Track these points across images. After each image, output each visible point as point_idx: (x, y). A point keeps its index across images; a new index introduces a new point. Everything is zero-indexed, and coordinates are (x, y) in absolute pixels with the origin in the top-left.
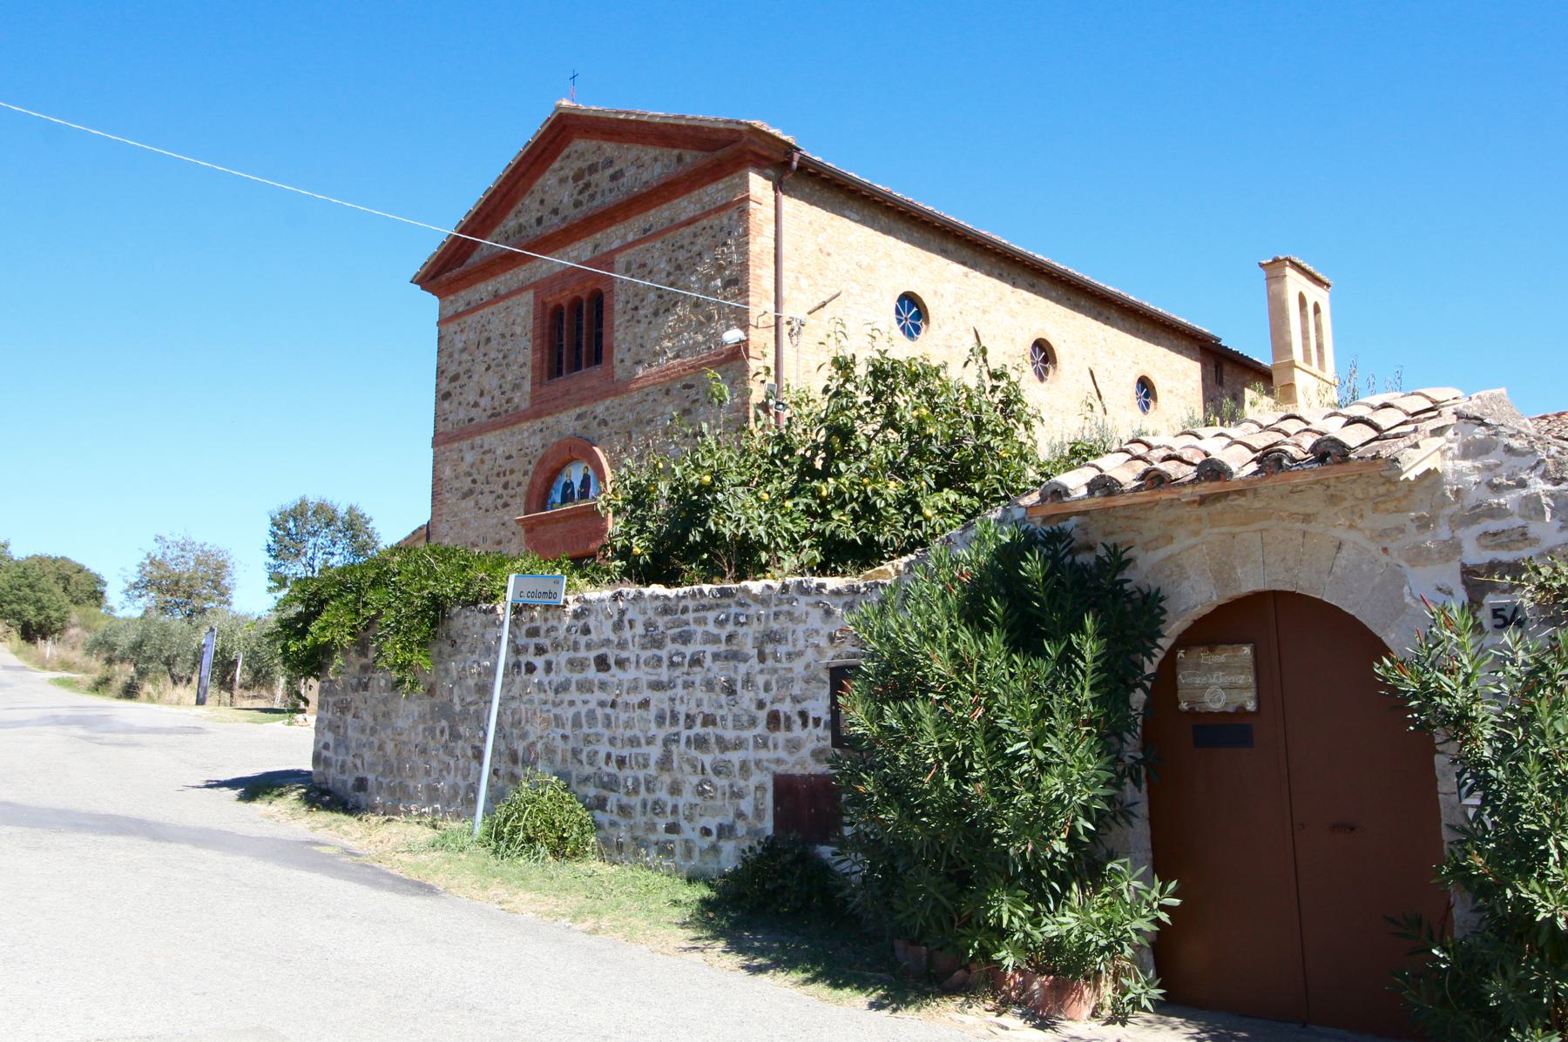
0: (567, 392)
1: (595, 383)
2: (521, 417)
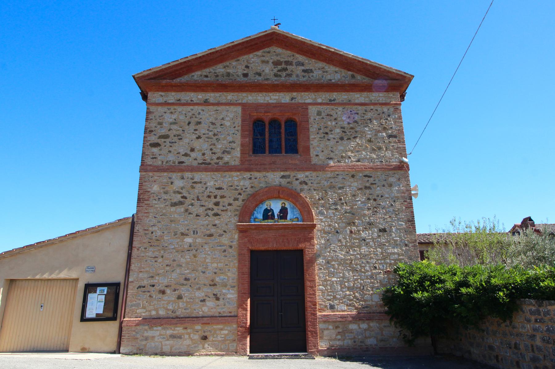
0: (274, 163)
1: (297, 162)
2: (228, 168)
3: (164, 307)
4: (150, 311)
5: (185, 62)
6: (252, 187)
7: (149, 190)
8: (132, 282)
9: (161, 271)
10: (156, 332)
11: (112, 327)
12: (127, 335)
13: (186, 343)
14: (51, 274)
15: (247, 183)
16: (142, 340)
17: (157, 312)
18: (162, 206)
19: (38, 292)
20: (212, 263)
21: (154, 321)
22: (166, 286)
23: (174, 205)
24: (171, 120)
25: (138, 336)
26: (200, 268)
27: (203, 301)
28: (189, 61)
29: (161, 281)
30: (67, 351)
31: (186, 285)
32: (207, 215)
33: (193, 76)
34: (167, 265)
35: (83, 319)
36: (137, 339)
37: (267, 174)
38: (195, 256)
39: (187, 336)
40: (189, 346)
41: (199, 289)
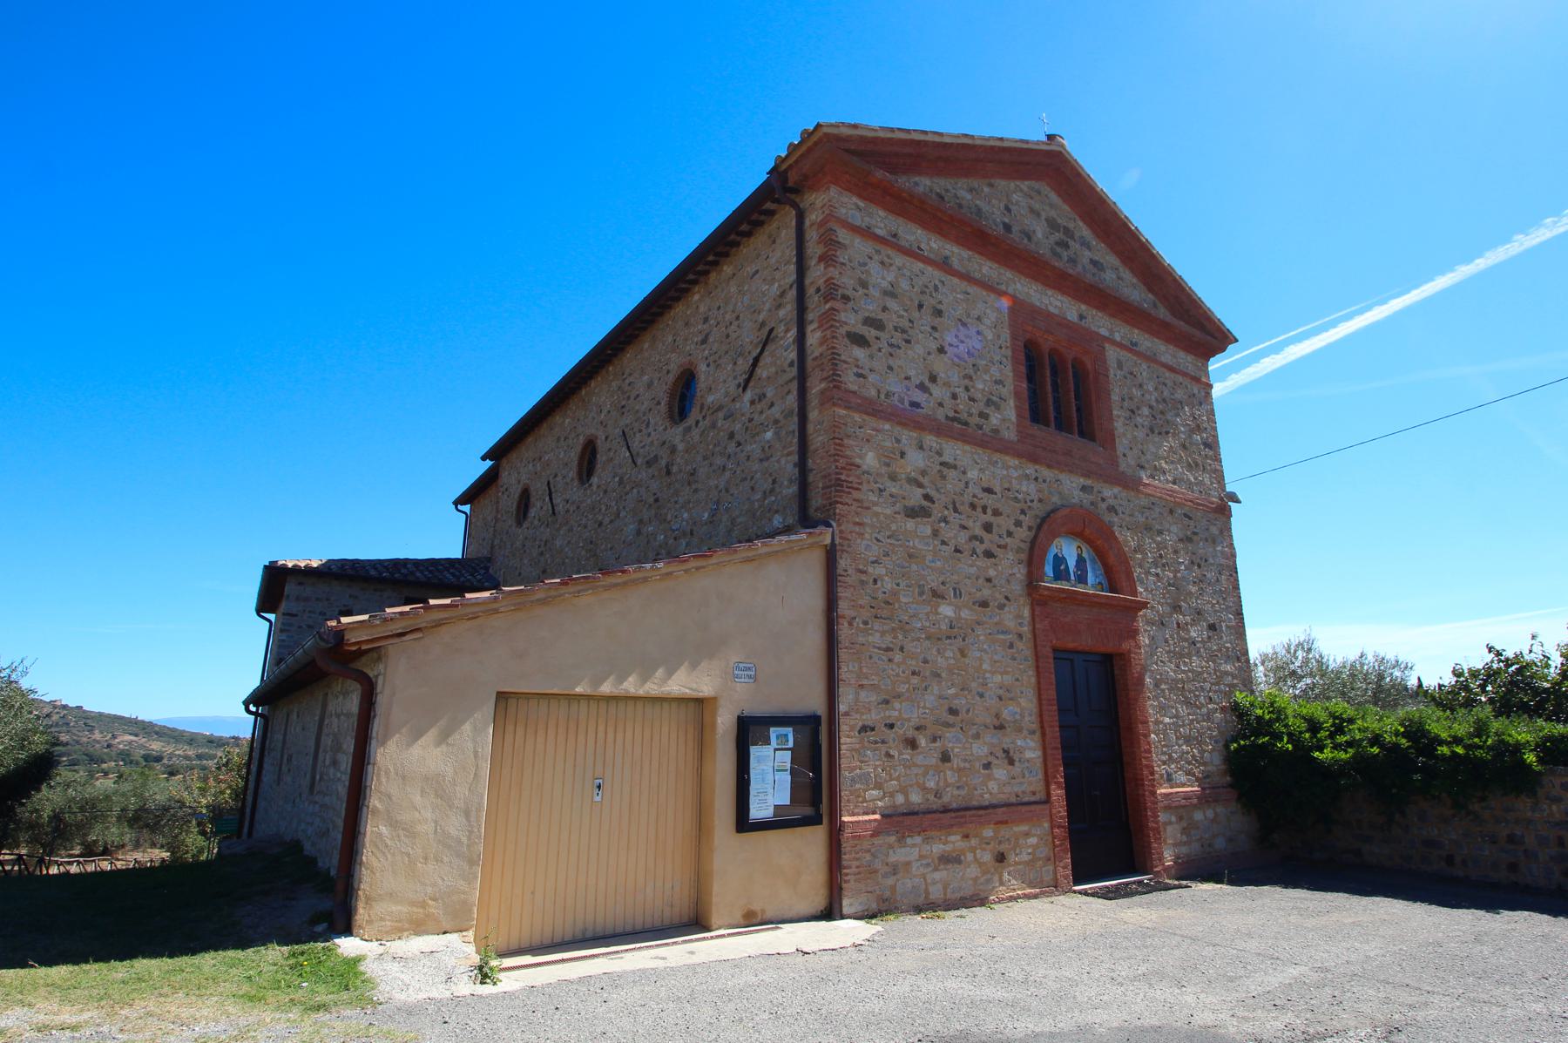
3: (918, 784)
4: (892, 795)
5: (919, 142)
6: (1040, 501)
7: (858, 461)
8: (847, 714)
9: (903, 688)
10: (912, 850)
11: (812, 842)
12: (855, 863)
13: (966, 876)
14: (644, 679)
15: (1029, 488)
16: (885, 876)
17: (906, 795)
18: (888, 511)
19: (581, 738)
20: (993, 673)
21: (908, 820)
22: (918, 729)
23: (912, 513)
24: (885, 284)
25: (878, 864)
26: (974, 685)
27: (987, 766)
28: (926, 143)
29: (907, 713)
30: (695, 923)
31: (953, 726)
32: (974, 552)
33: (916, 184)
34: (914, 673)
35: (743, 823)
36: (876, 871)
37: (1062, 476)
38: (963, 655)
39: (970, 857)
40: (975, 879)
41: (977, 736)
